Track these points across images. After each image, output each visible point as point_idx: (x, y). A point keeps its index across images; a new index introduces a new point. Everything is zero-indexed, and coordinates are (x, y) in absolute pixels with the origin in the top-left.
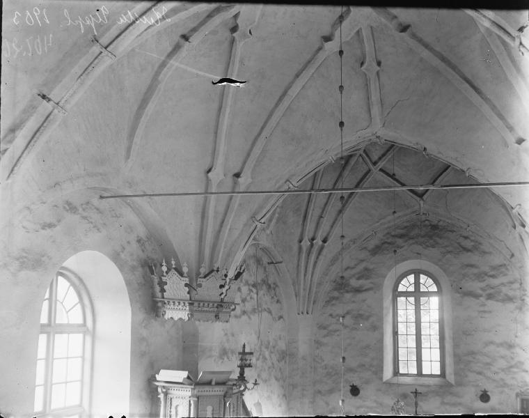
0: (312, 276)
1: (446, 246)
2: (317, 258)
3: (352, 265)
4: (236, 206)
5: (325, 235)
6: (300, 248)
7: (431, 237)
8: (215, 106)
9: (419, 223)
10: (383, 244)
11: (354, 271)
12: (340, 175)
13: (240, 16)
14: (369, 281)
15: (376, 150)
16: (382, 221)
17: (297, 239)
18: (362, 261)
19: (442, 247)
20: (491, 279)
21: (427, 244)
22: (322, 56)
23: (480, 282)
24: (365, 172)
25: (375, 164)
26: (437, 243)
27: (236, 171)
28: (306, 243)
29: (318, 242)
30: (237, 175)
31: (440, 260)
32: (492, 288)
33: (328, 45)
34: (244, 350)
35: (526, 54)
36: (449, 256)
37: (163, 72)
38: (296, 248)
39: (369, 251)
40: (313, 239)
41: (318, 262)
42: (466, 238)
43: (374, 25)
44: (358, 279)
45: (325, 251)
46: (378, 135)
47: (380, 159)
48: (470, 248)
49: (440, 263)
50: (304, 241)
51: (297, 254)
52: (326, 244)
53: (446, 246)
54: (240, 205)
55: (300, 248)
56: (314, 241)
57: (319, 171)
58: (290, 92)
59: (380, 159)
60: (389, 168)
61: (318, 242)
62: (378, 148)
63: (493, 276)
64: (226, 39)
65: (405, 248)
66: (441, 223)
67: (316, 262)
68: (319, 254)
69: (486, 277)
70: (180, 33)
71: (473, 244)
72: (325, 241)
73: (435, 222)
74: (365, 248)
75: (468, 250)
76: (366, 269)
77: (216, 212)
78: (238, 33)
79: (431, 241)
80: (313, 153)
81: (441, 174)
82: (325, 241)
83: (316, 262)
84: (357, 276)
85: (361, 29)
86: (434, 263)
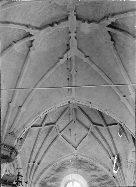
0: (32, 179)
1: (85, 168)
2: (35, 171)
3: (48, 176)
4: (18, 120)
5: (39, 161)
6: (28, 166)
7: (79, 165)
8: (17, 76)
9: (74, 160)
10: (61, 167)
11: (49, 179)
12: (47, 135)
13: (34, 41)
14: (55, 183)
15: (61, 126)
16: (61, 158)
17: (28, 162)
18: (52, 175)
19: (84, 169)
20: (102, 181)
21: (78, 167)
22: (59, 64)
23: (98, 182)
24: (56, 135)
25: (60, 132)
26: (82, 167)
27: (20, 105)
28: (31, 164)
29: (36, 164)
30: (21, 107)
31: (83, 174)
32: (103, 184)
33: (61, 60)
34: (20, 176)
35: (132, 42)
36: (86, 172)
37: (4, 52)
38: (27, 165)
39: (55, 170)
40: (34, 162)
41: (35, 173)
42: (92, 165)
43: (77, 55)
44: (51, 182)
45: (38, 168)
46: (74, 98)
47: (62, 130)
48: (94, 169)
49: (83, 175)
50: (31, 162)
51: (27, 168)
52: (39, 165)
53: (85, 168)
54: (19, 120)
55: (28, 166)
56: (35, 163)
57: (49, 113)
58: (45, 76)
59: (62, 130)
60: (65, 135)
61: (36, 164)
62: (62, 126)
63: (103, 180)
64: (27, 51)
65: (69, 169)
66: (82, 160)
67: (34, 173)
68: (36, 170)
69: (100, 180)
70: (13, 41)
71: (94, 167)
72: (38, 164)
73: (80, 159)
74: (54, 169)
75: (93, 170)
76: (54, 178)
77: (9, 121)
78: (32, 48)
79: (79, 166)
80: (50, 103)
81: (83, 139)
82: (38, 164)
83: (34, 173)
84: (50, 181)
85: (72, 56)
86: (80, 175)
